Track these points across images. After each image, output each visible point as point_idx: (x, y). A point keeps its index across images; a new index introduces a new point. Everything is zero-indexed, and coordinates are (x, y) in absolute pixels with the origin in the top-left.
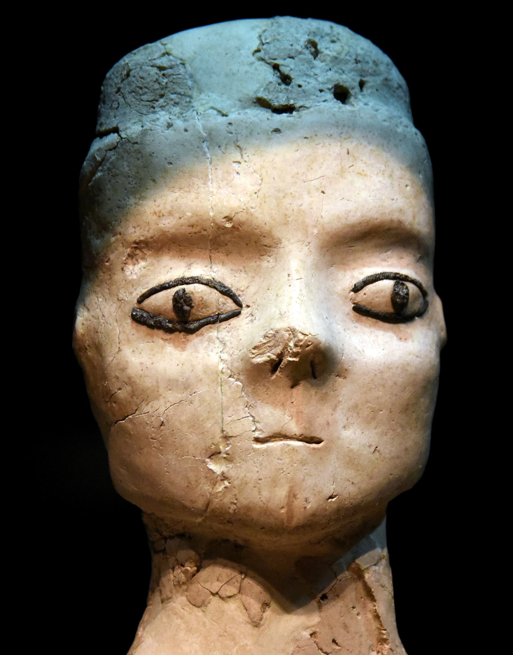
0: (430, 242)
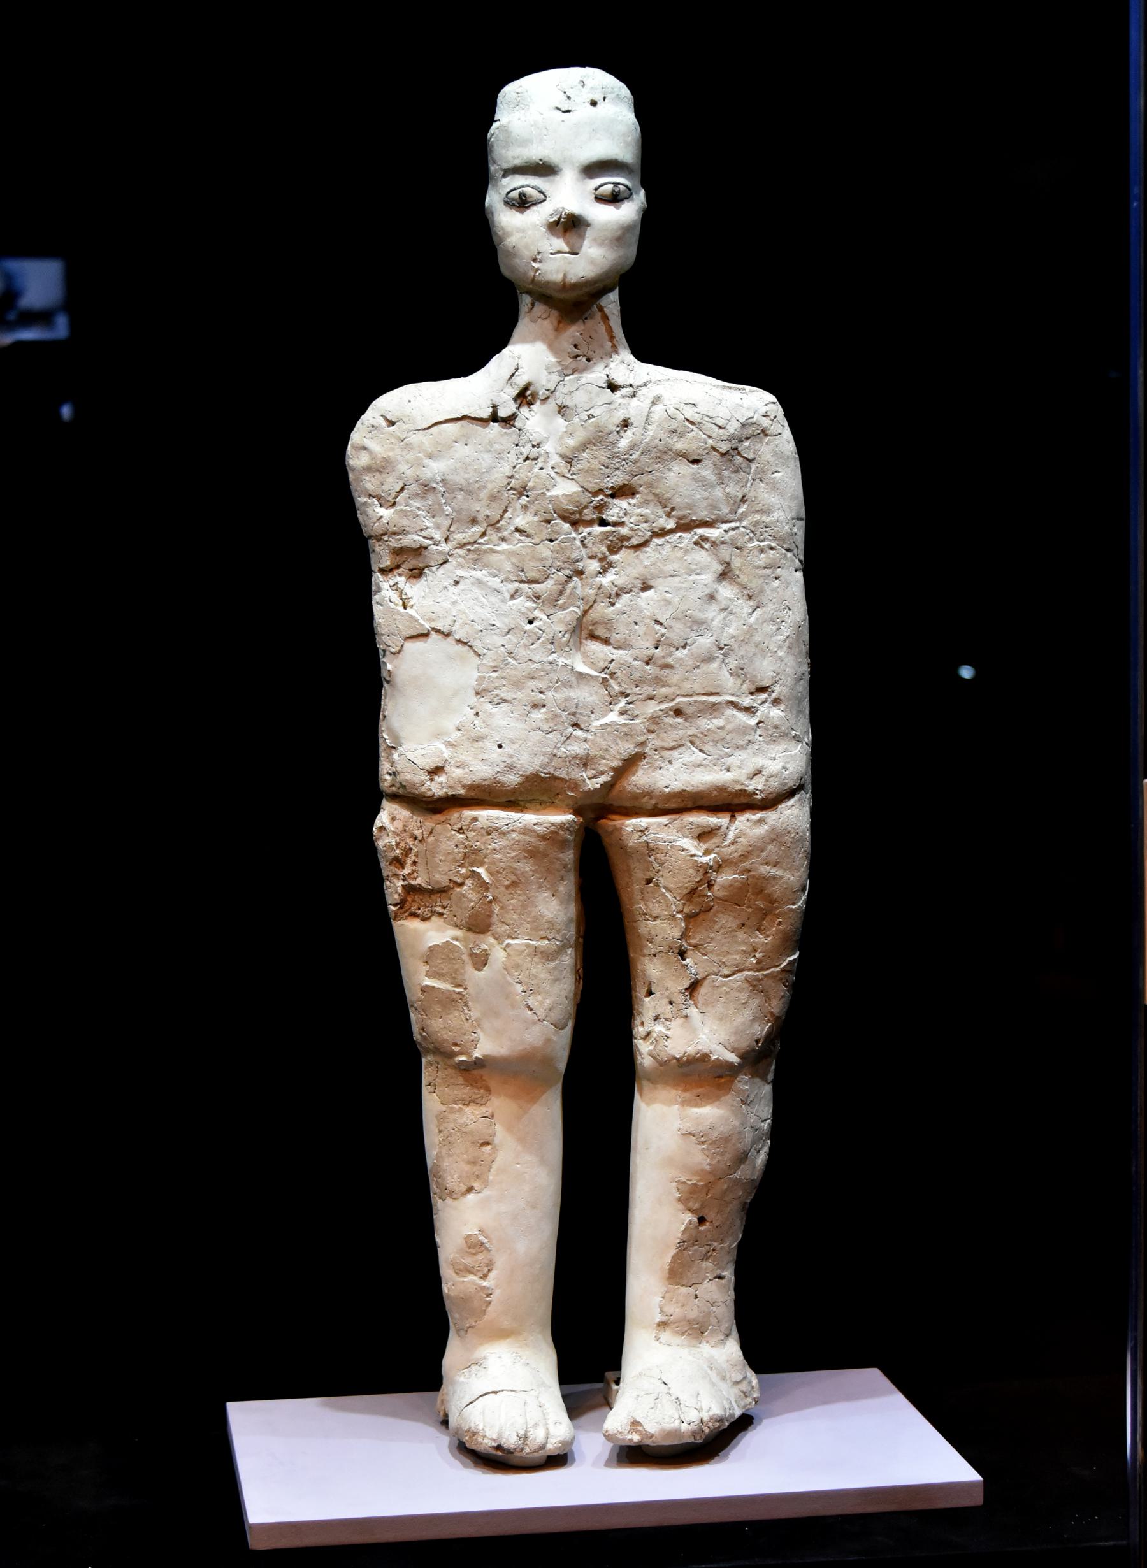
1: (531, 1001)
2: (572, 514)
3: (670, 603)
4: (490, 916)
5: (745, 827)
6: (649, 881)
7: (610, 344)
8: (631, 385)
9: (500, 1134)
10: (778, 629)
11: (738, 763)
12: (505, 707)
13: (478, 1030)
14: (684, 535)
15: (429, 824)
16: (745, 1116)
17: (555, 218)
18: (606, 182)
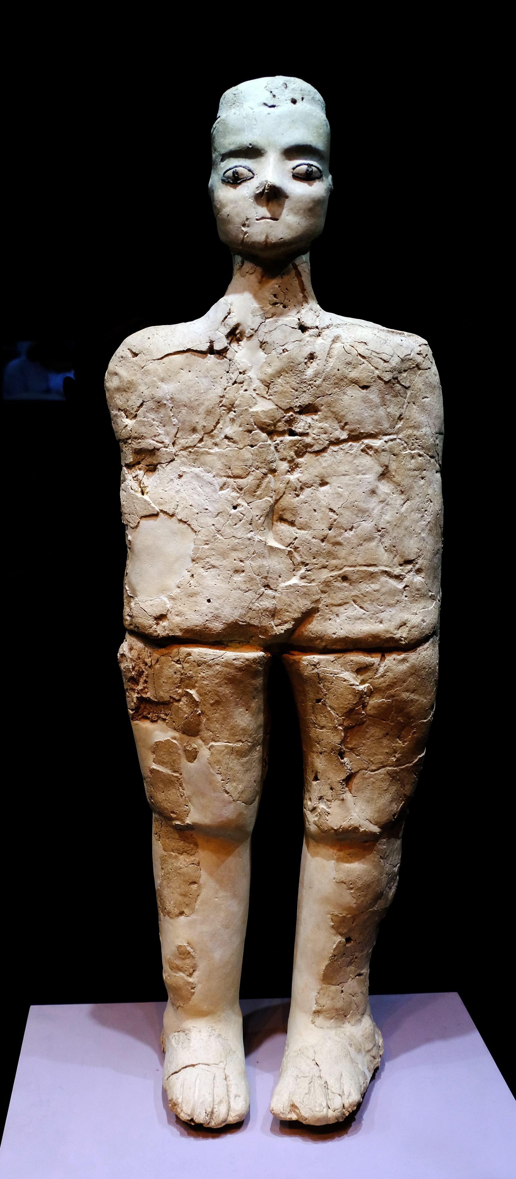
0: (327, 155)
1: (228, 787)
2: (268, 426)
3: (341, 496)
4: (199, 725)
5: (392, 664)
6: (319, 701)
7: (301, 295)
8: (317, 327)
9: (204, 877)
10: (423, 516)
11: (389, 617)
12: (213, 571)
13: (190, 804)
14: (354, 444)
15: (156, 655)
16: (383, 867)
17: (261, 190)
18: (302, 164)
